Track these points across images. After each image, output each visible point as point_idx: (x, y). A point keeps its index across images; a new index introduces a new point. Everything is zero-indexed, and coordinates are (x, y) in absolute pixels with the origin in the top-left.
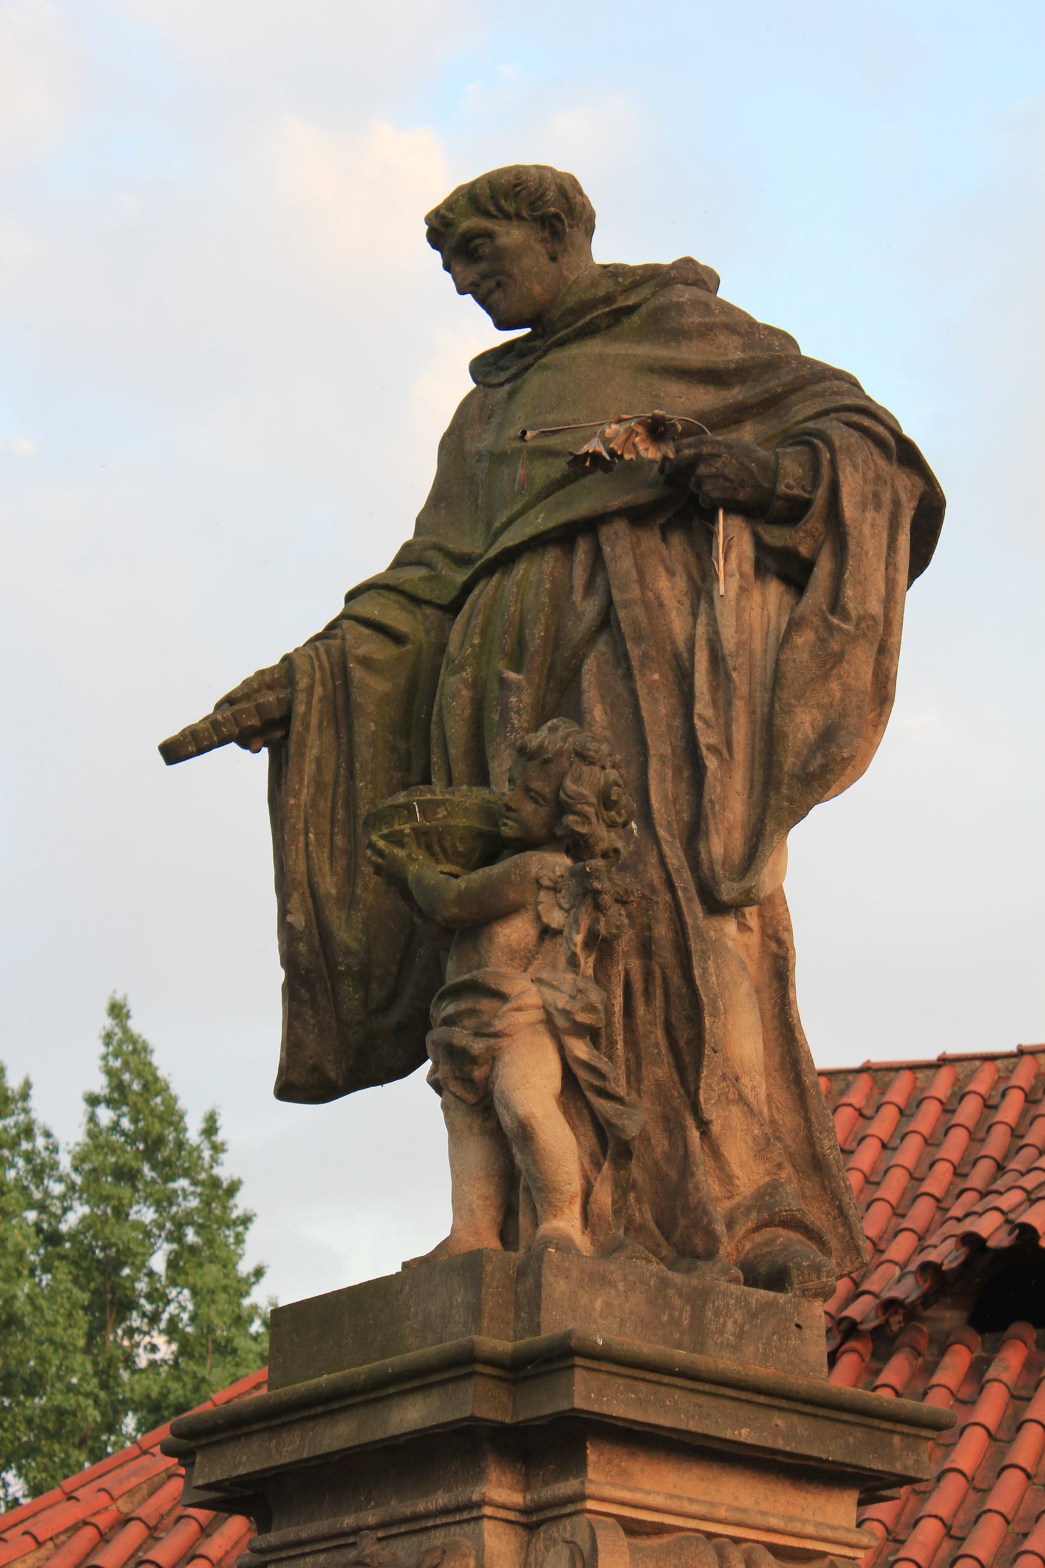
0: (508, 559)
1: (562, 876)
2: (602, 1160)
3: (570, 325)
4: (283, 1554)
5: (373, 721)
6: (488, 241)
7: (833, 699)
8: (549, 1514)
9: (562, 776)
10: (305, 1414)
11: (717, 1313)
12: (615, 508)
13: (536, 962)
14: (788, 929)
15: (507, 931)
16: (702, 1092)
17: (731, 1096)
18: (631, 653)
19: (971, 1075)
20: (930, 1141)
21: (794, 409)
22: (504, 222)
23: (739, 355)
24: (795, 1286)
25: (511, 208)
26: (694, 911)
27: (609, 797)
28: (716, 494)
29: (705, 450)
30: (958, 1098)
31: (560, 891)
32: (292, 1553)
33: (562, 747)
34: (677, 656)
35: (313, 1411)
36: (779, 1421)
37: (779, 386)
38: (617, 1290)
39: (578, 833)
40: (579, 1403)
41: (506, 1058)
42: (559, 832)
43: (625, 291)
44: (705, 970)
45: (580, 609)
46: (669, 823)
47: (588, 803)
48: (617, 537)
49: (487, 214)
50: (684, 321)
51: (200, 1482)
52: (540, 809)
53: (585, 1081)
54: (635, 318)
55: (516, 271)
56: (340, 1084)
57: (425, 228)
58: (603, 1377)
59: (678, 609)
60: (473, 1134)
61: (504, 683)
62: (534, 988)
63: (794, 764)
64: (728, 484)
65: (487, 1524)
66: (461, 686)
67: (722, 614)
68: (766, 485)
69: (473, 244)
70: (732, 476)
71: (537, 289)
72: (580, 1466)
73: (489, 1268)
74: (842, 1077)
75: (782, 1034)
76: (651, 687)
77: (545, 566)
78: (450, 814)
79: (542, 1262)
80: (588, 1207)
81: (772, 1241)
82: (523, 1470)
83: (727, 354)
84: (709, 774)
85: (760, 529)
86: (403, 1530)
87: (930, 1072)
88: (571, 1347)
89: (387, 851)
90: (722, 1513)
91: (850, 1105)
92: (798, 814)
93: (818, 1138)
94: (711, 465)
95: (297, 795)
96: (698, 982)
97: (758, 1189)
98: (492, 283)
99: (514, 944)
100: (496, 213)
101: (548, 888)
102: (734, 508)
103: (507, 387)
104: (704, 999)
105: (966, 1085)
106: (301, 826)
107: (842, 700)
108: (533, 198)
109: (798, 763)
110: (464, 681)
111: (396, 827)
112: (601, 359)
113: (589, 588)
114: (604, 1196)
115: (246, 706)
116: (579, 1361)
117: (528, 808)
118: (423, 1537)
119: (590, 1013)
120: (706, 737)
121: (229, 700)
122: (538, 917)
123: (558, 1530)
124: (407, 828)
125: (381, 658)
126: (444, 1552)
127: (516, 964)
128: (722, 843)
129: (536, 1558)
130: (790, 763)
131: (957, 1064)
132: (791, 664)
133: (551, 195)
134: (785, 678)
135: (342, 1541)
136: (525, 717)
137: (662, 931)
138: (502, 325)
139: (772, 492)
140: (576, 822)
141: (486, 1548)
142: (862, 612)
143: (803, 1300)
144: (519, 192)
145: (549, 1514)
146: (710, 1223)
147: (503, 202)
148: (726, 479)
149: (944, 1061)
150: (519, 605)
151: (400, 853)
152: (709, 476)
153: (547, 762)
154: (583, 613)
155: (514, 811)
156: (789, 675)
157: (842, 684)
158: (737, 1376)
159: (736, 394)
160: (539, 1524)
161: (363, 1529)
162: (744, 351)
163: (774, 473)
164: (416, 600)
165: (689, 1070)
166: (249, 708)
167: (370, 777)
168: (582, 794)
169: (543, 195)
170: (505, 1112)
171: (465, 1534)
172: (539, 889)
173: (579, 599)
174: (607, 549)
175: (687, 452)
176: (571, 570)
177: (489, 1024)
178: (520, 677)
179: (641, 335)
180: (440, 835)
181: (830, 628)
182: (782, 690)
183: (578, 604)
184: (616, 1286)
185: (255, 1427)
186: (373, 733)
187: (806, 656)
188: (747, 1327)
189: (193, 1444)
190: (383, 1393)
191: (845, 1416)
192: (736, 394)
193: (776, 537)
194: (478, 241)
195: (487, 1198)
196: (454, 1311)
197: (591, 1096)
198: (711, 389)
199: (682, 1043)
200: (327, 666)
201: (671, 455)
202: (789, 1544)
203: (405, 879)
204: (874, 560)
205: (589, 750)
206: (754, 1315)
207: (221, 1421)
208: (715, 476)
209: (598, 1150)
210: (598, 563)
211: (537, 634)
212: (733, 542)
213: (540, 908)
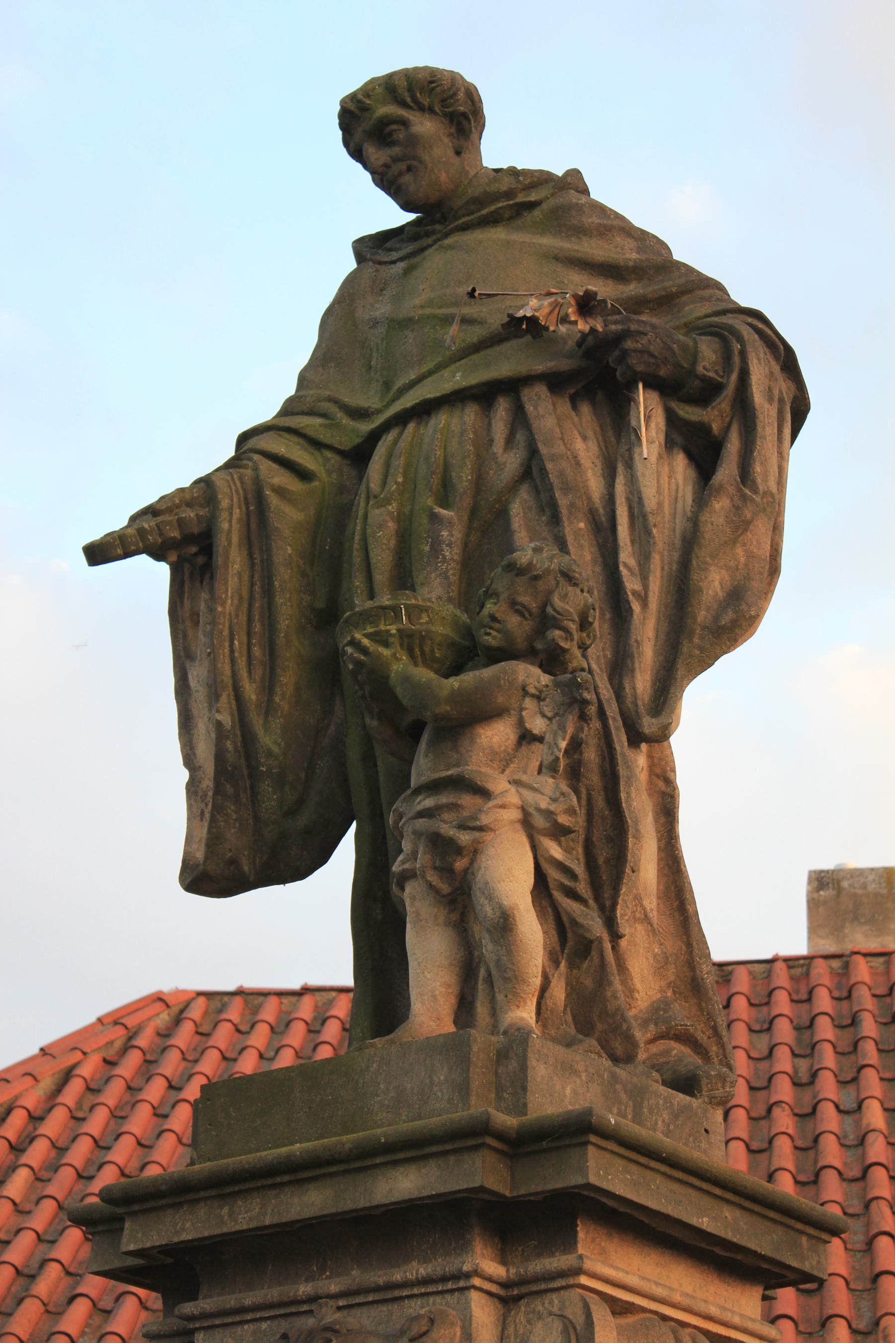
0: (424, 410)
1: (547, 686)
2: (560, 958)
3: (472, 213)
4: (217, 1322)
5: (289, 545)
6: (402, 128)
7: (739, 562)
8: (534, 1288)
9: (550, 593)
10: (269, 1181)
11: (651, 1111)
12: (539, 371)
13: (512, 766)
14: (673, 770)
15: (489, 733)
16: (619, 907)
17: (638, 915)
18: (560, 502)
19: (330, 1003)
20: (300, 1055)
21: (687, 308)
22: (418, 114)
23: (634, 256)
24: (704, 1093)
25: (426, 102)
26: (620, 739)
27: (587, 618)
28: (640, 368)
29: (633, 327)
30: (320, 1022)
31: (544, 700)
32: (229, 1320)
33: (549, 566)
34: (592, 512)
35: (278, 1180)
36: (728, 1213)
37: (674, 286)
38: (581, 1080)
39: (561, 647)
40: (593, 1179)
41: (491, 851)
42: (539, 645)
43: (524, 189)
44: (628, 793)
45: (501, 460)
46: (598, 657)
47: (573, 621)
48: (539, 398)
49: (403, 104)
50: (584, 220)
51: (132, 1247)
52: (525, 622)
53: (555, 880)
54: (537, 213)
55: (426, 158)
56: (252, 879)
57: (339, 108)
58: (608, 1156)
59: (593, 469)
60: (438, 925)
61: (434, 518)
62: (513, 789)
63: (706, 618)
64: (652, 360)
65: (474, 1295)
66: (388, 518)
67: (644, 475)
68: (685, 365)
70: (656, 354)
71: (443, 177)
72: (569, 1243)
73: (475, 1049)
74: (218, 997)
75: (668, 865)
76: (577, 533)
77: (466, 418)
78: (430, 622)
79: (527, 1045)
80: (543, 1002)
81: (666, 1053)
82: (499, 1246)
83: (624, 254)
84: (635, 617)
85: (674, 405)
86: (370, 1299)
87: (293, 999)
88: (591, 1123)
89: (372, 648)
90: (677, 1298)
91: (230, 1021)
92: (706, 662)
93: (698, 963)
94: (637, 341)
95: (223, 604)
96: (624, 805)
97: (652, 1004)
98: (403, 166)
99: (496, 746)
100: (412, 104)
101: (533, 696)
102: (653, 383)
103: (401, 265)
104: (629, 821)
105: (327, 1010)
106: (226, 633)
107: (746, 565)
108: (445, 96)
109: (709, 617)
110: (390, 514)
111: (382, 627)
112: (508, 244)
113: (510, 441)
114: (559, 992)
115: (169, 519)
116: (593, 1138)
117: (513, 621)
118: (396, 1306)
119: (570, 815)
120: (631, 584)
121: (150, 511)
122: (521, 722)
123: (543, 1304)
124: (393, 629)
125: (295, 489)
126: (432, 1321)
127: (495, 765)
128: (642, 683)
129: (515, 1330)
130: (702, 616)
131: (317, 994)
132: (709, 526)
133: (461, 95)
134: (704, 538)
135: (293, 1309)
136: (456, 550)
137: (591, 755)
138: (406, 207)
139: (692, 372)
140: (561, 637)
141: (474, 1318)
142: (766, 488)
143: (709, 1106)
144: (433, 89)
145: (534, 1288)
146: (629, 1029)
147: (418, 95)
148: (652, 355)
149: (306, 990)
150: (442, 450)
151: (385, 652)
152: (635, 351)
153: (536, 578)
154: (504, 464)
156: (707, 536)
157: (746, 551)
158: (706, 1167)
159: (632, 289)
160: (518, 1299)
161: (321, 1298)
162: (638, 253)
163: (695, 356)
164: (316, 444)
165: (605, 887)
166: (172, 521)
167: (288, 596)
168: (569, 611)
169: (455, 94)
170: (486, 902)
171: (447, 1304)
173: (500, 451)
174: (529, 408)
175: (613, 327)
176: (490, 424)
177: (475, 818)
178: (451, 513)
179: (543, 228)
180: (423, 638)
181: (744, 498)
183: (499, 455)
184: (580, 1076)
185: (202, 1194)
186: (290, 556)
187: (721, 520)
188: (672, 1127)
189: (121, 1210)
190: (368, 1162)
191: (772, 1214)
192: (632, 289)
193: (690, 413)
194: (394, 127)
195: (449, 986)
196: (436, 1089)
197: (557, 895)
198: (610, 282)
199: (601, 861)
200: (241, 492)
201: (600, 328)
202: (719, 1332)
203: (387, 678)
204: (770, 445)
205: (574, 571)
206: (676, 1117)
207: (164, 1188)
208: (642, 352)
209: (558, 948)
210: (519, 418)
211: (464, 478)
212: (648, 412)
213: (524, 713)
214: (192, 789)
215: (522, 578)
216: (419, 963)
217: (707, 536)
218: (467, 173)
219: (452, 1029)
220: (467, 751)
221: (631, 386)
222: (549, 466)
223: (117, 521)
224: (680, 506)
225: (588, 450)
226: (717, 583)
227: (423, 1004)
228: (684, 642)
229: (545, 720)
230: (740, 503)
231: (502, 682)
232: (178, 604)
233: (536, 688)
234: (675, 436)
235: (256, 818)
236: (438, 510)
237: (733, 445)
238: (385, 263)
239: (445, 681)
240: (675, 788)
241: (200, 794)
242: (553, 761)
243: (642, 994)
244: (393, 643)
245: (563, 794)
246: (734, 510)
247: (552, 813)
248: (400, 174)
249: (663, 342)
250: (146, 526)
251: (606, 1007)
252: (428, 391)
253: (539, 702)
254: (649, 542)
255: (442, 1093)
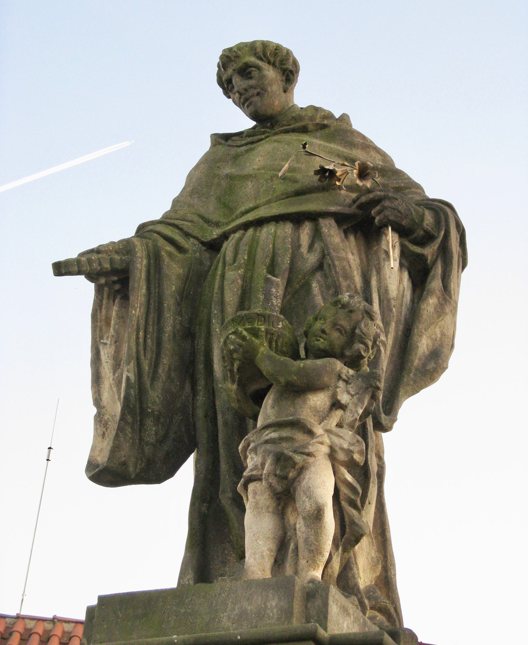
0: (260, 223)
1: (353, 376)
2: (340, 543)
12: (332, 211)
14: (383, 452)
15: (315, 399)
22: (266, 64)
31: (350, 384)
39: (362, 355)
41: (313, 469)
42: (348, 353)
47: (371, 340)
50: (354, 138)
52: (342, 337)
53: (345, 494)
55: (269, 89)
60: (269, 512)
61: (267, 280)
64: (400, 215)
66: (238, 277)
67: (390, 277)
69: (250, 69)
70: (402, 211)
71: (277, 103)
85: (407, 243)
99: (318, 407)
107: (441, 339)
110: (239, 275)
113: (311, 247)
117: (335, 335)
121: (97, 251)
124: (263, 328)
133: (291, 60)
134: (422, 318)
136: (279, 301)
148: (400, 212)
153: (351, 311)
155: (326, 334)
157: (441, 331)
172: (338, 380)
174: (325, 230)
177: (305, 446)
182: (420, 324)
194: (253, 69)
196: (268, 611)
197: (344, 504)
209: (339, 537)
210: (317, 234)
211: (285, 262)
213: (338, 390)
214: (98, 419)
215: (343, 310)
216: (254, 534)
217: (424, 317)
218: (288, 104)
219: (270, 576)
220: (301, 408)
221: (383, 226)
222: (337, 263)
223: (73, 255)
224: (405, 300)
225: (355, 260)
226: (425, 346)
227: (255, 559)
228: (405, 376)
229: (350, 396)
230: (443, 303)
231: (328, 368)
232: (98, 311)
233: (346, 375)
234: (403, 261)
235: (141, 439)
236: (269, 276)
237: (439, 269)
238: (233, 146)
239: (295, 362)
240: (384, 463)
241: (103, 423)
242: (353, 421)
243: (362, 580)
244: (262, 336)
245: (358, 441)
246: (439, 305)
247: (351, 451)
248: (253, 96)
249: (407, 206)
250: (93, 258)
251: (348, 583)
252: (263, 212)
253: (347, 385)
254: (390, 316)
255: (273, 614)
